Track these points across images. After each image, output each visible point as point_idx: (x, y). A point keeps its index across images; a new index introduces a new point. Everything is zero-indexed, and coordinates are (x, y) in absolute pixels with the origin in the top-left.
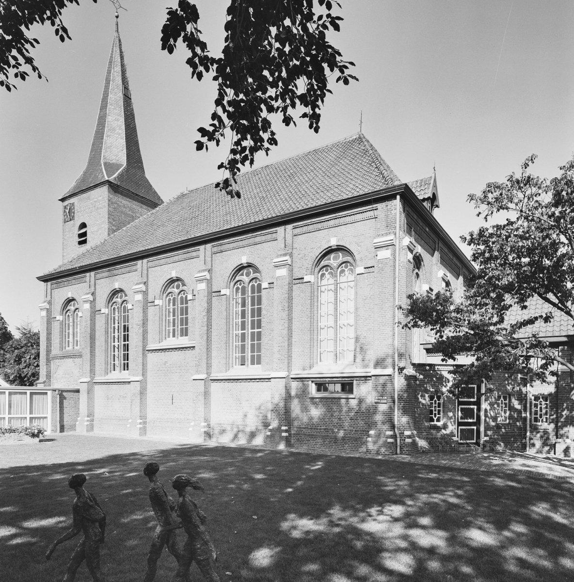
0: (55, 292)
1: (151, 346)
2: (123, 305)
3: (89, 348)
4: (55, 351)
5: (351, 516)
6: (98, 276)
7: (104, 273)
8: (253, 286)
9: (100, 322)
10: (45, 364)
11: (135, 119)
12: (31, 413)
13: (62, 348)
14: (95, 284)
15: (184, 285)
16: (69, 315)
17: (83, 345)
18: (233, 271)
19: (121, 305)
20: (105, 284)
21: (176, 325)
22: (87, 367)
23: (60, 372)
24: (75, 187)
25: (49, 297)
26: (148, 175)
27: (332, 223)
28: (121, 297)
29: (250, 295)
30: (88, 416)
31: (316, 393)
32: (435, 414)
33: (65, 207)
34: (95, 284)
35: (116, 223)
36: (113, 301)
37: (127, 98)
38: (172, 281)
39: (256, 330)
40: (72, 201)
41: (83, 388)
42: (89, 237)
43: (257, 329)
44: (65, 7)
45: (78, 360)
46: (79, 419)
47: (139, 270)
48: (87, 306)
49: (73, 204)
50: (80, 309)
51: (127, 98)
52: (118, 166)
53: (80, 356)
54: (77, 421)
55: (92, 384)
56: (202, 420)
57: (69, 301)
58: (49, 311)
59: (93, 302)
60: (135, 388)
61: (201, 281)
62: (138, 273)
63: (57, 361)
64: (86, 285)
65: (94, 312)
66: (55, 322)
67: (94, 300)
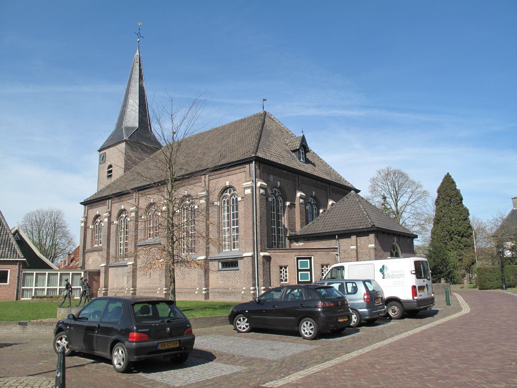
0: (90, 211)
1: (139, 243)
2: (232, 198)
3: (106, 245)
4: (88, 247)
6: (113, 202)
8: (233, 199)
9: (89, 232)
10: (82, 255)
12: (36, 286)
14: (111, 207)
15: (234, 190)
16: (121, 220)
17: (103, 245)
19: (231, 198)
20: (117, 206)
21: (230, 218)
23: (91, 260)
24: (101, 147)
25: (110, 209)
27: (227, 173)
28: (189, 201)
29: (231, 205)
30: (104, 288)
31: (222, 268)
32: (284, 277)
33: (101, 155)
34: (111, 207)
36: (121, 217)
37: (140, 70)
38: (225, 189)
39: (235, 227)
40: (106, 151)
43: (236, 226)
45: (101, 253)
46: (99, 289)
47: (134, 197)
48: (106, 220)
49: (105, 153)
50: (103, 221)
52: (133, 128)
53: (101, 250)
54: (98, 290)
55: (107, 268)
56: (164, 286)
57: (97, 216)
58: (86, 223)
59: (109, 218)
60: (129, 269)
61: (248, 188)
62: (134, 200)
63: (89, 253)
64: (106, 207)
65: (110, 223)
66: (89, 230)
67: (111, 215)
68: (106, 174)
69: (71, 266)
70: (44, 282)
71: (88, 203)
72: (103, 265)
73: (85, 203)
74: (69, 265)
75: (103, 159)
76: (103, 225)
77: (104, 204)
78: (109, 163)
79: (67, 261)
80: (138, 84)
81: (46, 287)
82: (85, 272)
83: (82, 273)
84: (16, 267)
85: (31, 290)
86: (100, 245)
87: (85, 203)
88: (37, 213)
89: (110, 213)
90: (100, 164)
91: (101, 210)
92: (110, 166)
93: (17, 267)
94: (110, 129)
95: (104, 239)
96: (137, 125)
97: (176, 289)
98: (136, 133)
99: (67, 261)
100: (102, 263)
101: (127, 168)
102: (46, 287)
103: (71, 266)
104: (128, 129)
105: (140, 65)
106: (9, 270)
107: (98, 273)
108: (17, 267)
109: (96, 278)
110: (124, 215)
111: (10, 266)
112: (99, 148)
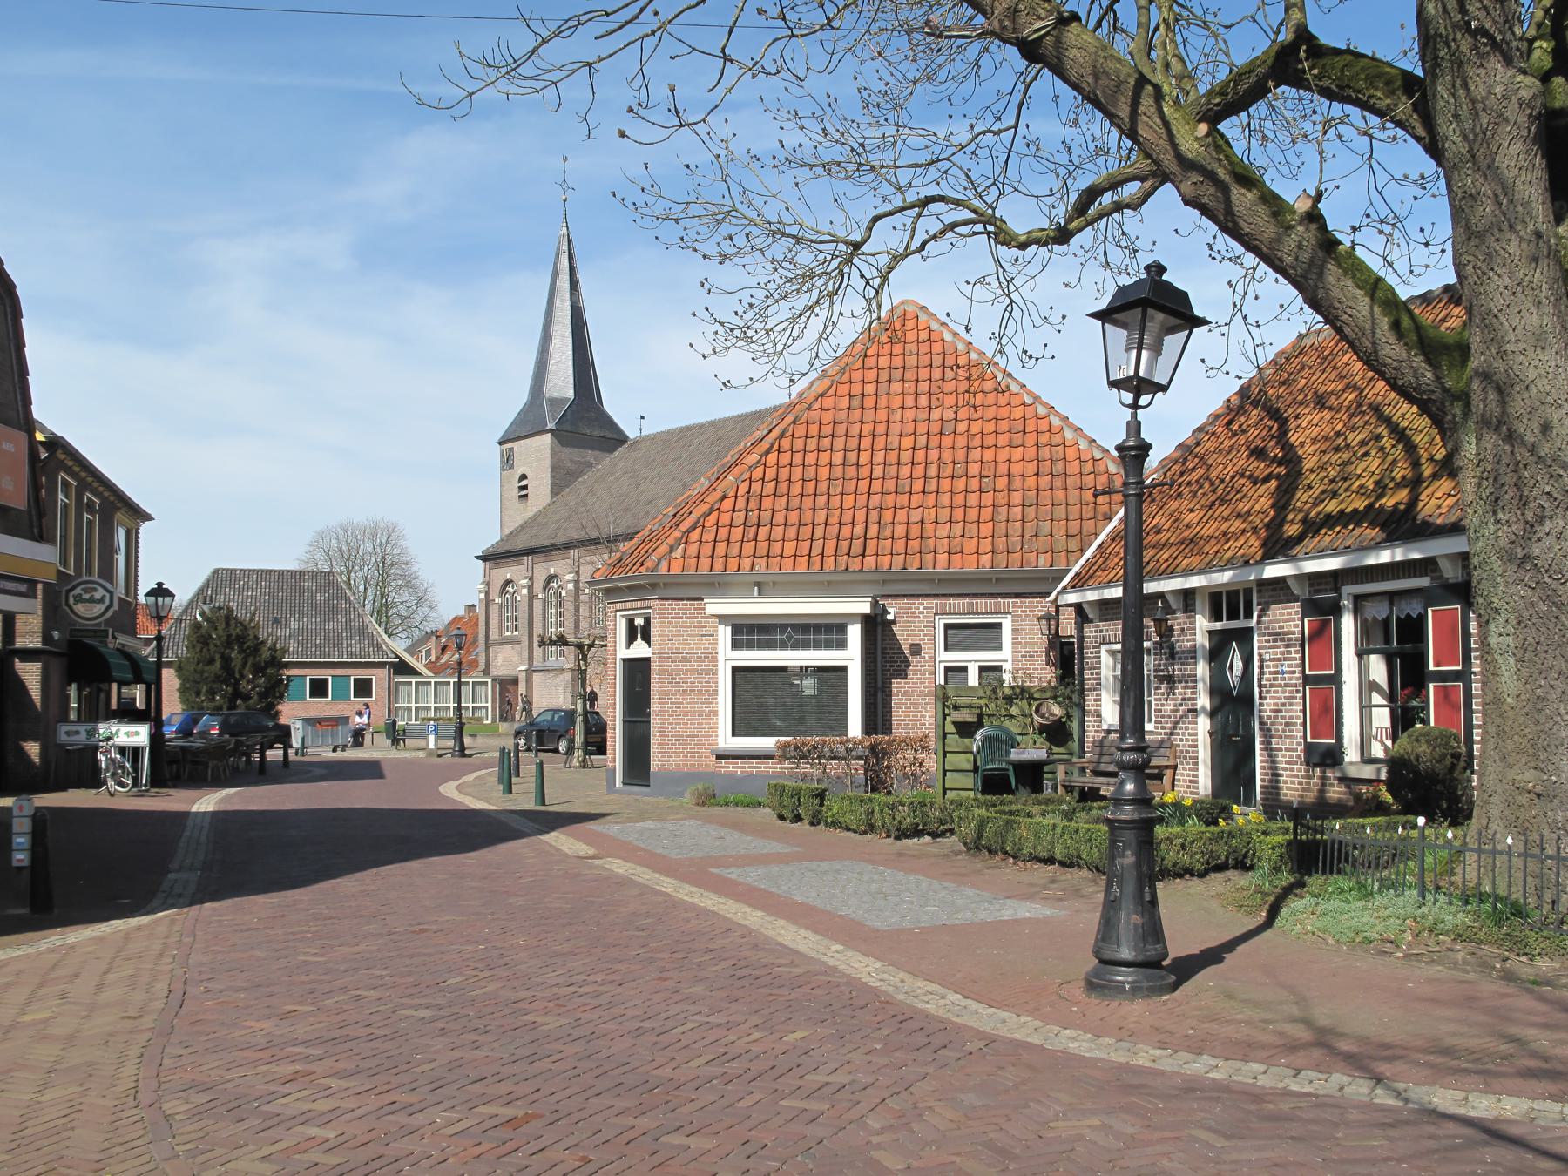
0: (494, 572)
4: (494, 636)
5: (1113, 460)
6: (536, 560)
7: (540, 557)
11: (199, 583)
13: (501, 634)
18: (6, 319)
20: (542, 569)
22: (526, 654)
23: (500, 659)
26: (1196, 951)
33: (502, 452)
35: (562, 479)
37: (572, 269)
41: (522, 677)
42: (529, 491)
44: (1462, 523)
45: (517, 647)
51: (572, 269)
52: (564, 400)
53: (519, 642)
55: (530, 672)
57: (508, 583)
58: (487, 593)
59: (530, 588)
64: (524, 567)
65: (532, 597)
68: (516, 493)
69: (443, 661)
70: (409, 695)
71: (491, 558)
72: (523, 668)
73: (485, 558)
74: (438, 659)
75: (508, 461)
76: (519, 598)
77: (520, 563)
78: (520, 471)
79: (433, 651)
80: (568, 303)
81: (433, 705)
82: (494, 680)
83: (490, 681)
84: (384, 673)
85: (409, 709)
86: (516, 633)
87: (485, 558)
88: (341, 532)
89: (531, 579)
90: (503, 469)
91: (514, 572)
92: (524, 477)
93: (385, 671)
94: (519, 397)
95: (522, 622)
96: (571, 394)
97: (1088, 648)
98: (569, 412)
99: (433, 651)
100: (521, 664)
101: (556, 490)
102: (433, 705)
103: (443, 661)
104: (554, 402)
105: (571, 258)
106: (726, 740)
107: (515, 681)
108: (385, 671)
109: (510, 688)
110: (555, 585)
111: (375, 671)
112: (498, 437)
